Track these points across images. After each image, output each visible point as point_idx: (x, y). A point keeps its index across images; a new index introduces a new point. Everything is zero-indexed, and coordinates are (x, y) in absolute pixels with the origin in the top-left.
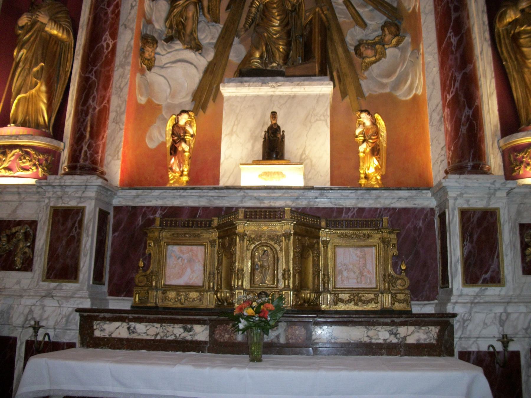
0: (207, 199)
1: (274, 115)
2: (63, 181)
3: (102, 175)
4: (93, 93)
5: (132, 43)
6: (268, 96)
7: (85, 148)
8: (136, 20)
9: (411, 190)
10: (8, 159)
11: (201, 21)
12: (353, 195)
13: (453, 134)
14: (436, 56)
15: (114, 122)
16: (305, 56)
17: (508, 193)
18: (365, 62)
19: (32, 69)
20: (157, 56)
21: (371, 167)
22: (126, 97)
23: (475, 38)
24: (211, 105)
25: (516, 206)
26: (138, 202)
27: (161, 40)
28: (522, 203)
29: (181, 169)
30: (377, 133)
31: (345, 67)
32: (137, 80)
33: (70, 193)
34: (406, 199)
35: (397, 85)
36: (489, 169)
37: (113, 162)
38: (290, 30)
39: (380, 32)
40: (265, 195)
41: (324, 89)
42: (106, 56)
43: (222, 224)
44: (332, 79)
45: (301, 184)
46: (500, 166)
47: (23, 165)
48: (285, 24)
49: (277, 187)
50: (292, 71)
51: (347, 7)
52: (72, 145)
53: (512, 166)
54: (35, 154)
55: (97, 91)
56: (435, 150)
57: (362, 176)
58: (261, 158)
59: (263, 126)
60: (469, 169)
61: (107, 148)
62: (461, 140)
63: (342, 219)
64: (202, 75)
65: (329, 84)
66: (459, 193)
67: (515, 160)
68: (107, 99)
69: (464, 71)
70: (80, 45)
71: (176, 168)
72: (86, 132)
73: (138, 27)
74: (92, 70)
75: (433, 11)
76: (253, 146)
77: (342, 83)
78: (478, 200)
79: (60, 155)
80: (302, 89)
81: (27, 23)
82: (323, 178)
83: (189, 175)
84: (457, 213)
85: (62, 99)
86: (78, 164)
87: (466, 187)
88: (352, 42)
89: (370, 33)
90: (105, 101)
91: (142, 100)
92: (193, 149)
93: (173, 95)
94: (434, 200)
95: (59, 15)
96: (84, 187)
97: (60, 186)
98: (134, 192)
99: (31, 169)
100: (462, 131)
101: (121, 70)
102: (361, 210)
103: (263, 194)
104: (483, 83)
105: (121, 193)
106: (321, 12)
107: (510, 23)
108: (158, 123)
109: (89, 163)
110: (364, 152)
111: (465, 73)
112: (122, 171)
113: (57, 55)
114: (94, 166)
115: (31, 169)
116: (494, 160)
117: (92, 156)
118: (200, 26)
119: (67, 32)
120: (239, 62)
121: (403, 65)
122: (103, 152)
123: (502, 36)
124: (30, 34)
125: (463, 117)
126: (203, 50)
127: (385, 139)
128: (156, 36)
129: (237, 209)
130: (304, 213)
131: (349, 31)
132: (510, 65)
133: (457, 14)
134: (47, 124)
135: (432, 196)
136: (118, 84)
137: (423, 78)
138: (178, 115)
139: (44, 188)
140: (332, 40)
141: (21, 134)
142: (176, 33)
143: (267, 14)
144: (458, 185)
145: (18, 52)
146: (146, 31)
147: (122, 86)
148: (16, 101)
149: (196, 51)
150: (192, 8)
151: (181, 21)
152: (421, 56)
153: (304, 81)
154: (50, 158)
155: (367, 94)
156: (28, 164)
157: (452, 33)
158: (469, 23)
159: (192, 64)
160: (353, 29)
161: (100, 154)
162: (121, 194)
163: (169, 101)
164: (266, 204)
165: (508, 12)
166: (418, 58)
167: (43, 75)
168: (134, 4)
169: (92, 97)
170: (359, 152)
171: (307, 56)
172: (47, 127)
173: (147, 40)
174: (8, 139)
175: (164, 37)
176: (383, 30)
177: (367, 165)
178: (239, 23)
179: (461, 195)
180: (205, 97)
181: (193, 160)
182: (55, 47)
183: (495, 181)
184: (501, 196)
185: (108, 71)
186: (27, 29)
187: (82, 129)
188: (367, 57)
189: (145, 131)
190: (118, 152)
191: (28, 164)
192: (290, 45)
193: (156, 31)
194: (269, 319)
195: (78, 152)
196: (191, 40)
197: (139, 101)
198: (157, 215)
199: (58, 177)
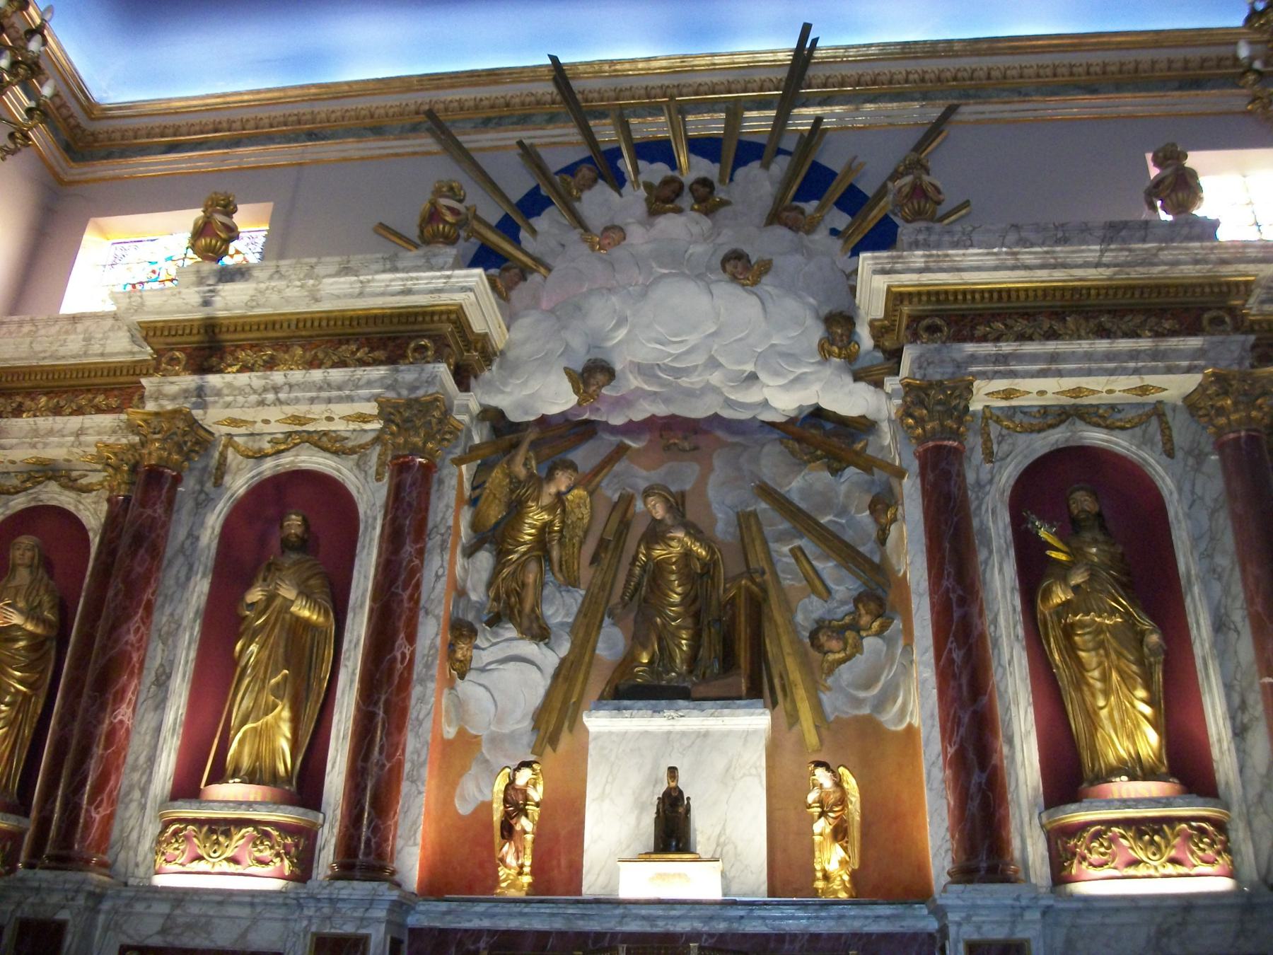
1: (673, 771)
5: (438, 641)
10: (233, 844)
17: (1044, 914)
21: (833, 861)
22: (429, 737)
24: (565, 740)
26: (450, 922)
27: (481, 622)
28: (1073, 926)
30: (843, 801)
32: (444, 701)
37: (407, 849)
40: (660, 913)
41: (754, 721)
45: (716, 894)
47: (258, 854)
50: (702, 690)
51: (797, 559)
56: (936, 840)
57: (819, 875)
60: (983, 872)
64: (549, 682)
65: (763, 713)
66: (963, 915)
67: (1065, 849)
71: (511, 860)
82: (753, 875)
83: (532, 873)
84: (961, 947)
87: (974, 907)
88: (806, 624)
93: (500, 719)
95: (312, 582)
98: (443, 906)
103: (658, 911)
105: (422, 907)
110: (821, 834)
113: (307, 650)
118: (546, 592)
121: (892, 665)
128: (470, 617)
129: (614, 935)
140: (771, 619)
147: (421, 717)
150: (533, 567)
153: (722, 708)
155: (832, 718)
156: (267, 854)
159: (532, 663)
160: (806, 600)
162: (422, 908)
163: (493, 728)
164: (661, 927)
170: (813, 834)
171: (728, 662)
173: (461, 630)
174: (235, 809)
176: (856, 607)
177: (826, 856)
180: (555, 721)
190: (415, 832)
191: (267, 854)
194: (928, 427)
198: (482, 945)
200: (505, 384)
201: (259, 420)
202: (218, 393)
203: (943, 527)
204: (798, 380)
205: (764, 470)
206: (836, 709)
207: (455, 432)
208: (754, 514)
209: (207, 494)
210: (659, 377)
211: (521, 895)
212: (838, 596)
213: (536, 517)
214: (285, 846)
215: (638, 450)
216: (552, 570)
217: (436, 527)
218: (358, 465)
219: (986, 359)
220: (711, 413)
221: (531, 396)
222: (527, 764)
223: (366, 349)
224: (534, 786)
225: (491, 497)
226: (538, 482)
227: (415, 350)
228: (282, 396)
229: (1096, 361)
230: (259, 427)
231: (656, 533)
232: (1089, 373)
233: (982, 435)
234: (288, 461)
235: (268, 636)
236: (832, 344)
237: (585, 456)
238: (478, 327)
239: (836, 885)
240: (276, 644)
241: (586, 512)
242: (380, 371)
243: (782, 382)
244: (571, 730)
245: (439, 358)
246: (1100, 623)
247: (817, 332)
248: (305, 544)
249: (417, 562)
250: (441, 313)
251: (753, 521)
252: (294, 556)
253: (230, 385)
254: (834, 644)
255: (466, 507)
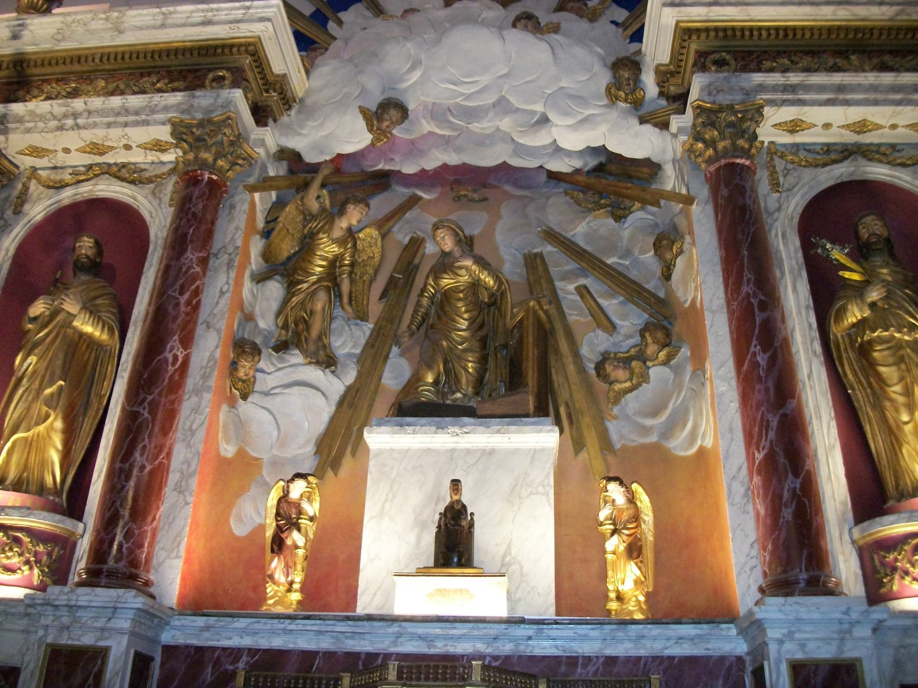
0: (333, 637)
2: (75, 597)
3: (145, 588)
4: (144, 440)
5: (218, 354)
6: (447, 450)
7: (119, 538)
8: (226, 316)
9: (700, 623)
11: (336, 317)
12: (595, 633)
13: (768, 521)
14: (734, 383)
15: (175, 489)
16: (510, 383)
17: (875, 630)
18: (614, 390)
19: (43, 390)
20: (258, 375)
21: (627, 580)
22: (201, 448)
23: (798, 351)
24: (347, 463)
25: (892, 651)
26: (208, 639)
27: (268, 347)
29: (290, 579)
30: (636, 518)
31: (580, 400)
32: (222, 416)
33: (84, 620)
34: (692, 640)
35: (669, 430)
36: (838, 584)
37: (168, 562)
38: (487, 336)
39: (637, 339)
40: (438, 631)
41: (542, 439)
42: (172, 377)
43: (358, 686)
44: (558, 422)
45: (502, 612)
46: (856, 575)
47: (5, 561)
48: (477, 326)
49: (460, 617)
50: (488, 407)
51: (582, 297)
52: (97, 531)
53: (879, 576)
54: (31, 542)
55: (150, 436)
56: (739, 552)
57: (612, 595)
58: (432, 564)
59: (436, 504)
60: (802, 585)
61: (159, 536)
62: (784, 530)
63: (575, 677)
64: (334, 408)
65: (552, 431)
66: (785, 631)
67: (883, 564)
68: (166, 450)
69: (781, 412)
70: (129, 354)
71: (279, 576)
72: (124, 508)
73: (230, 326)
74: (145, 399)
75: (725, 307)
76: (419, 538)
77: (574, 426)
78: (821, 644)
79: (74, 545)
80: (506, 439)
81: (44, 312)
82: (541, 599)
83: (302, 590)
84: (784, 668)
85: (91, 443)
86: (105, 567)
87: (799, 620)
88: (592, 357)
89: (622, 341)
90: (164, 454)
91: (228, 450)
92: (313, 541)
93: (282, 442)
94: (742, 641)
95: (99, 301)
96: (110, 610)
97: (66, 606)
98: (201, 621)
99: (20, 569)
100: (784, 518)
101: (194, 399)
102: (611, 661)
103: (436, 630)
104: (816, 428)
105: (177, 622)
106: (537, 307)
107: (853, 325)
108: (253, 491)
109: (125, 566)
110: (614, 553)
111: (784, 415)
112: (183, 579)
113: (89, 368)
114: (133, 570)
115: (20, 569)
116: (846, 566)
117: (131, 551)
118: (334, 326)
119: (109, 328)
120: (399, 388)
121: (679, 393)
122: (151, 545)
123: (842, 347)
124: (46, 331)
125: (786, 493)
126: (338, 366)
127: (651, 528)
128: (258, 341)
129: (387, 656)
130: (506, 670)
131: (586, 337)
132: (860, 395)
133: (765, 315)
134: (59, 486)
135: (738, 635)
136: (188, 424)
137: (712, 419)
138: (288, 482)
139: (39, 608)
140: (557, 351)
141: (10, 504)
142: (293, 336)
143: (447, 308)
144: (784, 617)
145: (24, 360)
146: (243, 334)
147: (195, 426)
148: (9, 444)
149: (326, 368)
150: (322, 296)
151: (304, 318)
152: (708, 382)
153: (508, 425)
154: (56, 550)
155: (618, 446)
156: (15, 561)
157: (758, 347)
158: (785, 328)
159: (317, 389)
160: (592, 334)
161: (146, 550)
162: (177, 623)
163: (275, 452)
164: (440, 648)
165: (849, 307)
166: (703, 384)
167: (61, 403)
168: (224, 290)
169: (141, 446)
172: (58, 492)
173: (244, 348)
175: (273, 342)
176: (643, 336)
177: (620, 576)
178: (400, 321)
179: (790, 634)
180: (337, 447)
181: (312, 559)
182: (87, 354)
183: (849, 608)
184: (862, 635)
185: (173, 402)
186: (43, 322)
187: (118, 504)
188: (617, 381)
189: (230, 506)
190: (179, 544)
191: (15, 561)
192: (487, 362)
193: (260, 331)
195: (106, 544)
196: (318, 350)
197: (223, 453)
198: (241, 665)
199: (66, 589)
200: (302, 128)
201: (59, 149)
202: (20, 120)
203: (740, 236)
204: (585, 120)
205: (551, 217)
206: (622, 437)
207: (249, 160)
208: (540, 255)
209: (6, 221)
210: (452, 123)
211: (290, 611)
212: (623, 331)
213: (328, 248)
214: (36, 554)
215: (429, 201)
216: (342, 305)
217: (224, 247)
218: (153, 193)
219: (774, 89)
220: (500, 161)
221: (327, 137)
222: (299, 476)
223: (166, 81)
224: (310, 500)
225: (285, 231)
226: (330, 216)
227: (214, 80)
228: (81, 121)
229: (881, 92)
230: (61, 159)
231: (445, 264)
232: (876, 103)
233: (768, 167)
234: (87, 190)
235: (48, 349)
236: (619, 90)
237: (382, 204)
238: (277, 67)
239: (631, 606)
240: (55, 356)
241: (377, 251)
242: (177, 98)
243: (571, 121)
244: (353, 454)
245: (235, 84)
246: (900, 340)
247: (604, 78)
248: (94, 267)
249: (198, 269)
250: (240, 45)
251: (539, 261)
252: (84, 277)
253: (32, 113)
254: (621, 374)
255: (258, 237)
